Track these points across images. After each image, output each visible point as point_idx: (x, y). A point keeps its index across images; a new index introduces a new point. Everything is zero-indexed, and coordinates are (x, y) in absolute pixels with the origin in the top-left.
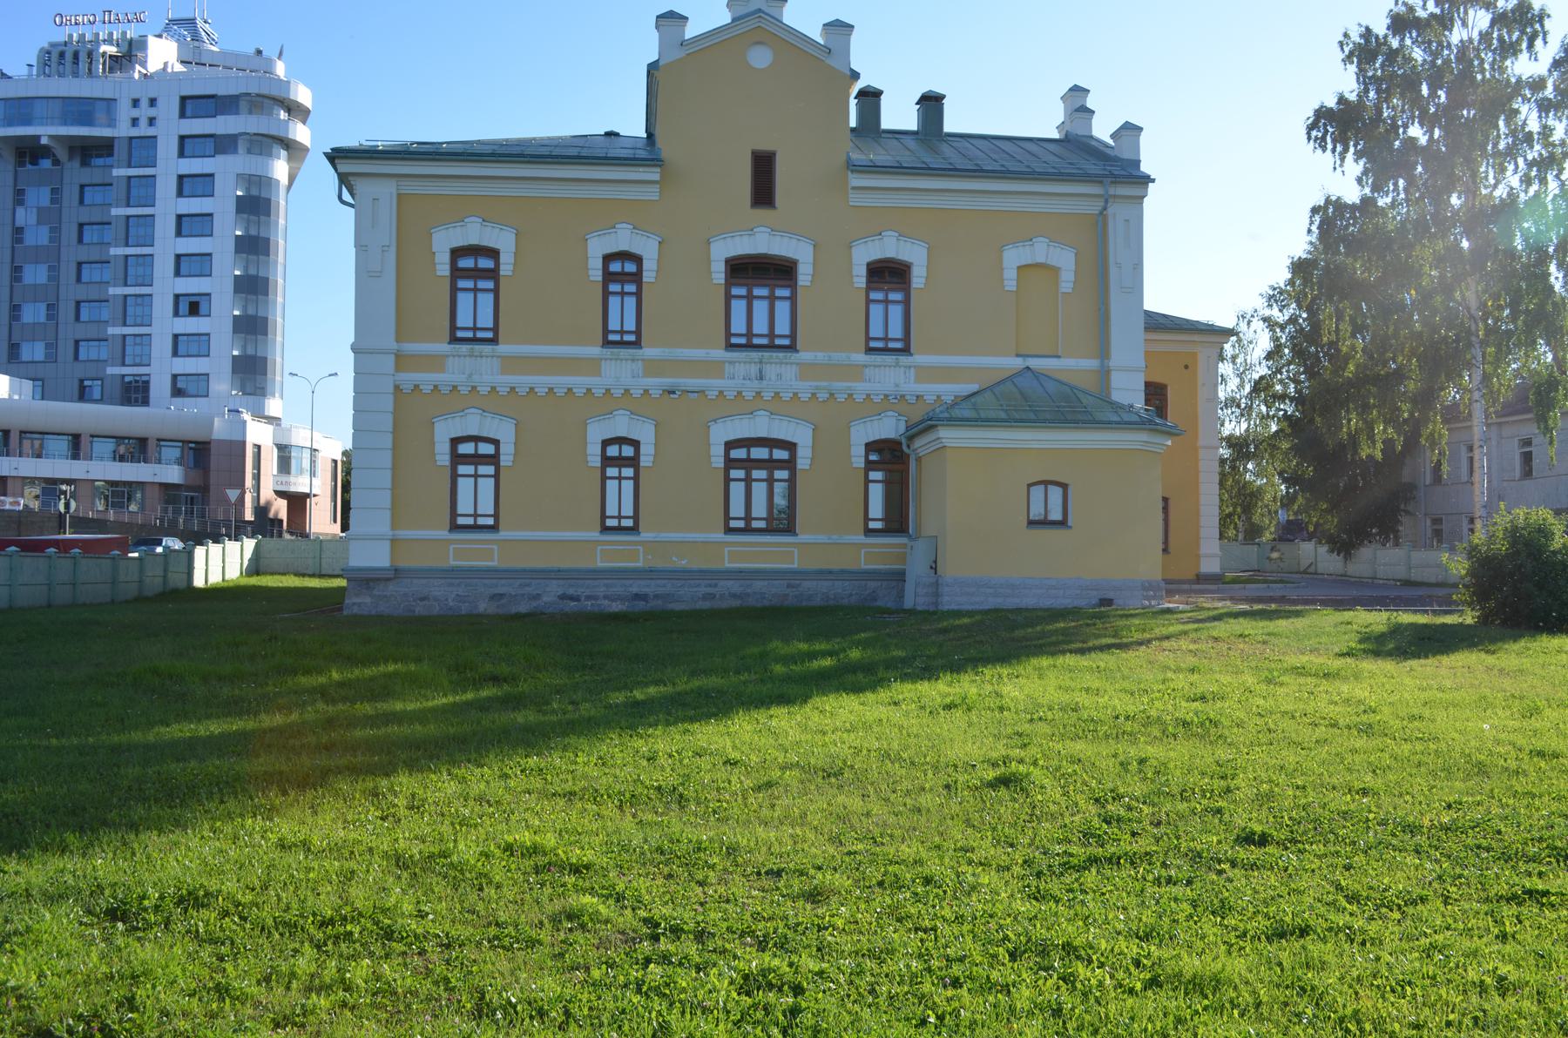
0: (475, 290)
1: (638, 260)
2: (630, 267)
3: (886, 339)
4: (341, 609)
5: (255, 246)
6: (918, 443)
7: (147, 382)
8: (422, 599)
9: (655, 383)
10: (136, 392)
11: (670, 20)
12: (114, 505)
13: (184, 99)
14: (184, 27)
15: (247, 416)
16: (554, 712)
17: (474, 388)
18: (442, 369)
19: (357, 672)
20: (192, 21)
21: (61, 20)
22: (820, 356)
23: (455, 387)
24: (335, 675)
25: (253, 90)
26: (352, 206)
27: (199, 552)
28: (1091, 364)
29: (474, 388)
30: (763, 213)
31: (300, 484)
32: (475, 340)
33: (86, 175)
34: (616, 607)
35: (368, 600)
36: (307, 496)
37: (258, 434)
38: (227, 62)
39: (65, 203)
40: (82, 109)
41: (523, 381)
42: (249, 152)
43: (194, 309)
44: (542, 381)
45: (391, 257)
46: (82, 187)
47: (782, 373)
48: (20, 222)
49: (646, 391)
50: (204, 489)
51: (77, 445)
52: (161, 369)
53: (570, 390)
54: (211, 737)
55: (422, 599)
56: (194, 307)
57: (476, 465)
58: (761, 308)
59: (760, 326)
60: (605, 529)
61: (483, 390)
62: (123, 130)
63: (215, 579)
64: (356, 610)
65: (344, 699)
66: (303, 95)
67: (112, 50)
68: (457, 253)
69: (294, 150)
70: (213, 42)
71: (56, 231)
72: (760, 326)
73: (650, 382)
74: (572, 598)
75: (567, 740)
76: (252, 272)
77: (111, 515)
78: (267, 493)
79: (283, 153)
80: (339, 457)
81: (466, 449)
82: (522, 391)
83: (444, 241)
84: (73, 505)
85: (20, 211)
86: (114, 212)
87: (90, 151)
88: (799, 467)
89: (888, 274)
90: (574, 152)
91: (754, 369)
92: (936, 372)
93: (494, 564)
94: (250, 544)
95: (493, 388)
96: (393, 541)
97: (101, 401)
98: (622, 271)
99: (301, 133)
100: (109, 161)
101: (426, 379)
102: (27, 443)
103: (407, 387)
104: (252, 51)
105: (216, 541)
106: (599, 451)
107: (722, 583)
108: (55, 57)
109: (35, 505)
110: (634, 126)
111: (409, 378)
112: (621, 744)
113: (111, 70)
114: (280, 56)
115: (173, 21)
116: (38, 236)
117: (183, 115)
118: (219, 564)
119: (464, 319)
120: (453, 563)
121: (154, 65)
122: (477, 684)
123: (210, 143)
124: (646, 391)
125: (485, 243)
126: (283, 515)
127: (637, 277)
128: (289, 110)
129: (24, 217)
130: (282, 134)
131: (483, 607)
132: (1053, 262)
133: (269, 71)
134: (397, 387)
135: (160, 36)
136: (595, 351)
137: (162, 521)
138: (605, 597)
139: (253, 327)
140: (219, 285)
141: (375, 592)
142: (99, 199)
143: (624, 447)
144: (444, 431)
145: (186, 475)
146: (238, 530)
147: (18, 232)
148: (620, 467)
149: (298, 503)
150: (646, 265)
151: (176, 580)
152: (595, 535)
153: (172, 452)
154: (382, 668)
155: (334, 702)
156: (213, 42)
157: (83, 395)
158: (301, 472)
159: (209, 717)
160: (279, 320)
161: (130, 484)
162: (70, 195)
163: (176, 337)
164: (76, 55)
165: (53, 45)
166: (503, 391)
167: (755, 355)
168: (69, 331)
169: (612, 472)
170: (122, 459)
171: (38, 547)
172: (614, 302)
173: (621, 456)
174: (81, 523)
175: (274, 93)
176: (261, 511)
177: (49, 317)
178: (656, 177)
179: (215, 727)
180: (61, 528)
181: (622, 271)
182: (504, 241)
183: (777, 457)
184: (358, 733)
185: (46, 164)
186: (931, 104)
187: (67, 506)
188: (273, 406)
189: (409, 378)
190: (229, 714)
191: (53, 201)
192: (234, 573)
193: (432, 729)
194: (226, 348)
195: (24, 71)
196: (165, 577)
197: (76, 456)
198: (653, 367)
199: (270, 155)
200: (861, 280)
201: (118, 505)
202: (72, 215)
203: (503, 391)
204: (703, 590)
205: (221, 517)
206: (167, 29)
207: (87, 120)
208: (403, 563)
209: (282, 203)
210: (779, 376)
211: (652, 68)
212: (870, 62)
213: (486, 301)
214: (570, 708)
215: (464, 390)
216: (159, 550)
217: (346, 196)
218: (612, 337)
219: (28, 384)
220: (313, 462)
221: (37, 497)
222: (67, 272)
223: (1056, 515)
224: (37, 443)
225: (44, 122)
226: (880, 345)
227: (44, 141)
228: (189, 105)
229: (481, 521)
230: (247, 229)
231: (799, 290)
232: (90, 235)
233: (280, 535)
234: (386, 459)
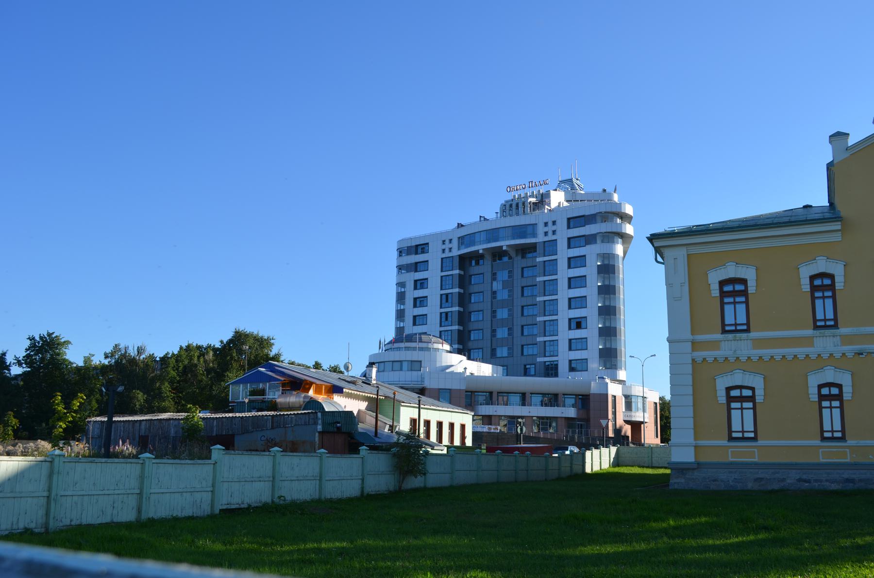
0: (735, 303)
1: (831, 277)
2: (827, 282)
4: (668, 485)
5: (608, 290)
7: (557, 365)
8: (714, 481)
9: (849, 349)
10: (551, 370)
12: (543, 429)
13: (569, 219)
14: (567, 184)
15: (608, 381)
16: (806, 549)
17: (738, 358)
18: (718, 349)
19: (684, 521)
20: (571, 180)
21: (510, 189)
23: (726, 358)
24: (672, 523)
25: (603, 210)
26: (663, 263)
27: (588, 454)
29: (738, 358)
31: (638, 417)
32: (736, 331)
33: (524, 263)
34: (834, 487)
35: (683, 481)
36: (642, 423)
37: (614, 389)
38: (590, 198)
39: (515, 278)
40: (521, 231)
41: (766, 352)
42: (603, 242)
43: (579, 326)
44: (778, 352)
45: (686, 288)
46: (523, 268)
48: (495, 289)
49: (844, 354)
50: (587, 420)
51: (524, 398)
52: (564, 357)
53: (795, 356)
54: (608, 554)
55: (714, 481)
56: (578, 324)
57: (741, 402)
60: (824, 439)
61: (744, 359)
62: (540, 238)
63: (596, 468)
64: (676, 487)
65: (679, 537)
66: (629, 209)
67: (533, 200)
68: (722, 283)
69: (625, 238)
70: (581, 189)
71: (511, 291)
73: (845, 348)
74: (806, 481)
75: (817, 568)
76: (607, 303)
77: (542, 435)
78: (620, 422)
79: (620, 240)
80: (657, 401)
81: (735, 393)
82: (766, 358)
83: (715, 278)
84: (524, 429)
85: (495, 283)
86: (538, 279)
87: (525, 250)
90: (787, 219)
93: (756, 460)
94: (614, 450)
95: (749, 358)
96: (696, 447)
97: (534, 375)
98: (822, 284)
99: (629, 229)
100: (534, 254)
101: (710, 355)
102: (501, 398)
103: (699, 360)
104: (601, 190)
105: (597, 448)
106: (817, 392)
108: (508, 207)
109: (505, 430)
110: (821, 199)
111: (699, 355)
112: (854, 572)
113: (534, 210)
114: (615, 192)
115: (562, 182)
116: (503, 295)
117: (569, 227)
118: (599, 460)
119: (729, 319)
120: (731, 459)
121: (554, 204)
122: (757, 530)
123: (583, 240)
124: (844, 354)
125: (738, 276)
126: (629, 434)
127: (832, 287)
128: (621, 218)
129: (497, 286)
130: (619, 231)
131: (750, 485)
133: (610, 199)
134: (693, 360)
135: (556, 190)
136: (810, 332)
137: (566, 437)
138: (827, 481)
139: (609, 332)
140: (591, 312)
142: (530, 274)
143: (832, 389)
144: (722, 384)
145: (578, 414)
146: (605, 442)
147: (494, 293)
148: (830, 401)
149: (637, 426)
150: (837, 279)
151: (577, 469)
152: (817, 442)
153: (570, 401)
154: (698, 520)
155: (673, 538)
156: (581, 189)
157: (526, 373)
158: (637, 410)
159: (605, 543)
160: (622, 328)
161: (547, 418)
162: (517, 272)
163: (570, 340)
164: (517, 205)
165: (507, 202)
166: (755, 359)
168: (518, 341)
169: (825, 404)
170: (546, 405)
171: (508, 451)
172: (819, 303)
173: (831, 394)
174: (528, 439)
175: (614, 210)
176: (617, 431)
177: (509, 334)
178: (839, 227)
179: (609, 549)
180: (518, 440)
181: (822, 284)
182: (749, 274)
184: (690, 556)
185: (506, 259)
187: (521, 430)
188: (622, 375)
189: (699, 355)
190: (616, 542)
191: (509, 277)
192: (606, 466)
193: (716, 556)
194: (596, 344)
195: (494, 216)
196: (571, 467)
197: (524, 404)
198: (847, 340)
199: (613, 242)
201: (545, 429)
202: (518, 283)
203: (755, 359)
205: (596, 435)
206: (559, 186)
207: (523, 236)
208: (702, 460)
209: (621, 266)
211: (830, 166)
213: (741, 308)
214: (816, 547)
215: (732, 360)
216: (568, 452)
217: (659, 259)
218: (819, 324)
219: (500, 368)
220: (644, 404)
221: (505, 426)
222: (517, 311)
224: (505, 398)
225: (504, 239)
226: (822, 323)
227: (504, 248)
228: (572, 222)
229: (746, 435)
230: (603, 282)
231: (750, 297)
232: (527, 292)
233: (628, 445)
234: (690, 400)
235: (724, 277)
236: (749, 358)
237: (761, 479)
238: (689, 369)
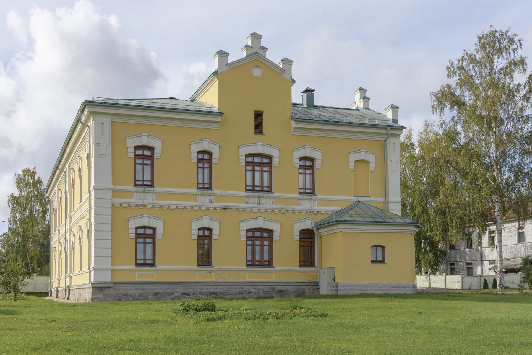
1: (210, 154)
3: (143, 181)
6: (321, 231)
8: (125, 295)
11: (222, 54)
22: (282, 195)
28: (382, 199)
30: (259, 136)
32: (143, 185)
47: (268, 203)
55: (125, 295)
58: (257, 175)
59: (257, 182)
72: (257, 182)
83: (132, 143)
88: (157, 238)
91: (257, 200)
92: (329, 201)
101: (125, 201)
107: (245, 287)
132: (367, 159)
134: (113, 205)
138: (200, 294)
141: (105, 292)
167: (256, 194)
183: (266, 235)
204: (238, 290)
208: (117, 280)
210: (266, 203)
223: (380, 259)
226: (141, 183)
229: (147, 262)
235: (248, 153)
236: (153, 206)
237: (158, 293)
238: (109, 211)
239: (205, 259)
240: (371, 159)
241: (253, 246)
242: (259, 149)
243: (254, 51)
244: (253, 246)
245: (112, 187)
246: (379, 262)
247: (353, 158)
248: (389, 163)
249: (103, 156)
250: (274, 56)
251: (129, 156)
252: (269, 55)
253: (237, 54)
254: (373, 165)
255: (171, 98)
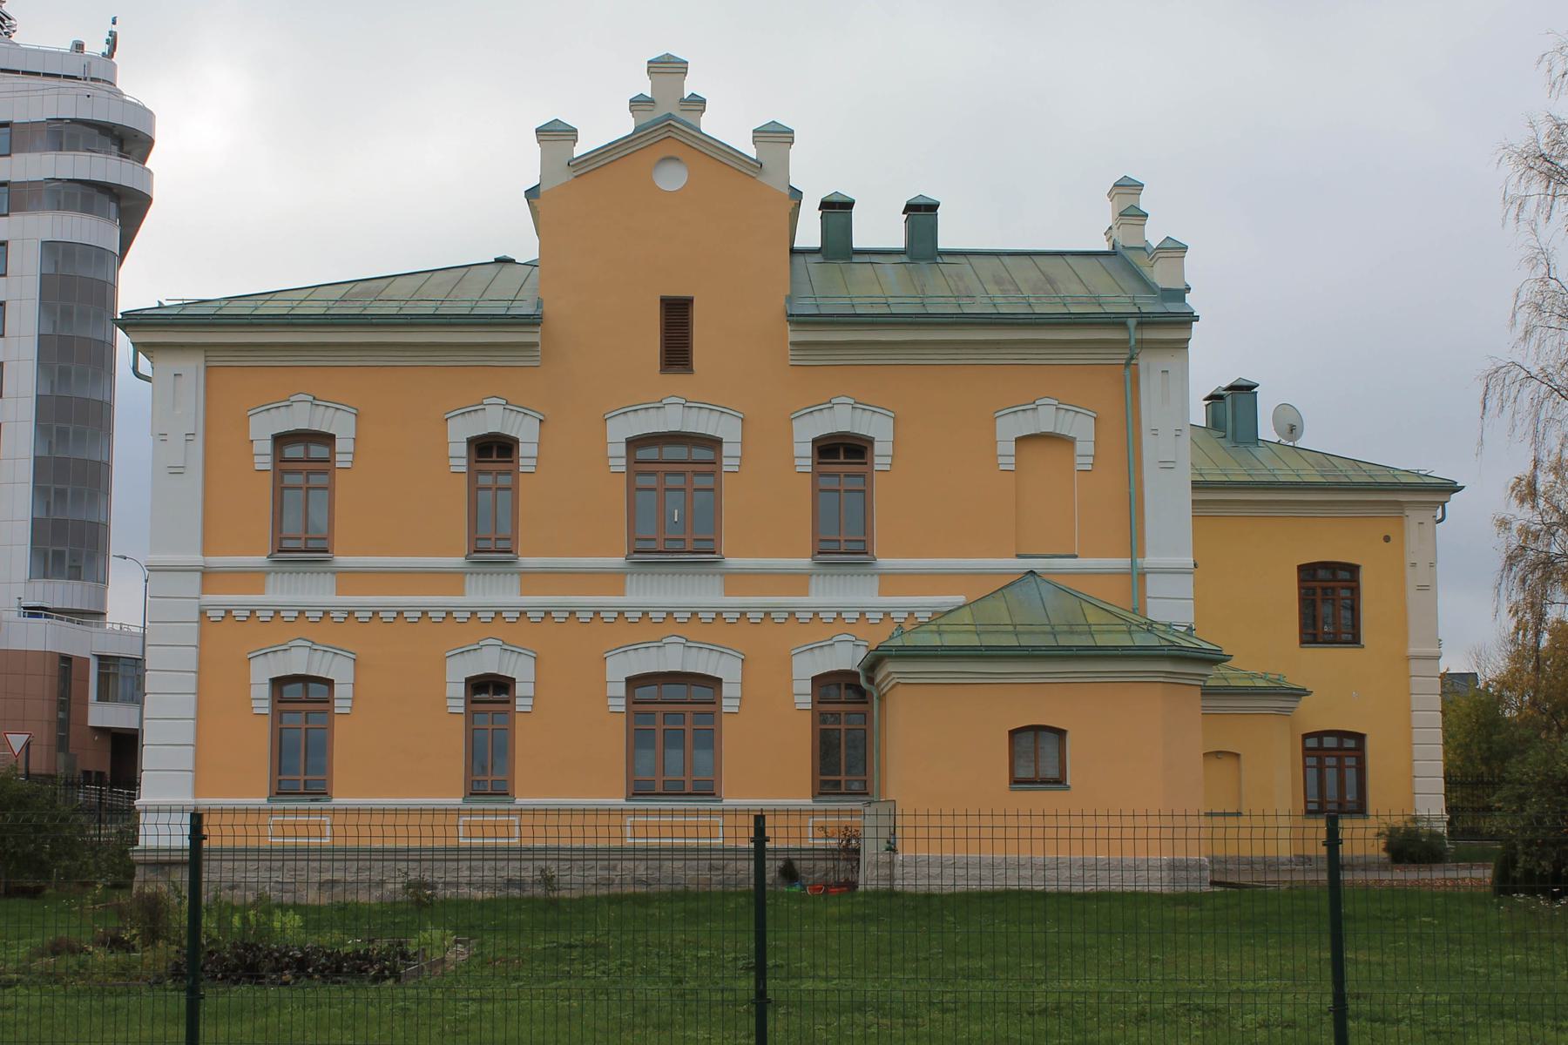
11: (554, 134)
30: (676, 380)
45: (198, 446)
68: (280, 440)
83: (264, 427)
89: (842, 450)
104: (66, 46)
134: (203, 613)
186: (921, 213)
200: (805, 463)
212: (812, 175)
238: (191, 633)
239: (488, 776)
240: (1080, 427)
241: (1321, 769)
242: (671, 419)
243: (659, 113)
244: (1321, 769)
245: (197, 559)
246: (1045, 781)
247: (1009, 428)
248: (1147, 438)
249: (177, 471)
250: (730, 125)
251: (258, 467)
252: (711, 124)
253: (603, 124)
254: (1085, 446)
255: (498, 261)
